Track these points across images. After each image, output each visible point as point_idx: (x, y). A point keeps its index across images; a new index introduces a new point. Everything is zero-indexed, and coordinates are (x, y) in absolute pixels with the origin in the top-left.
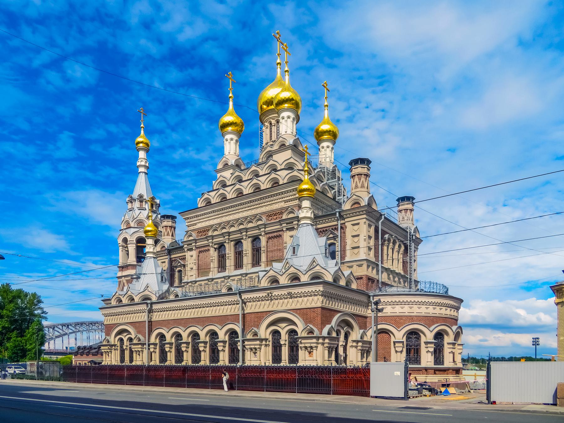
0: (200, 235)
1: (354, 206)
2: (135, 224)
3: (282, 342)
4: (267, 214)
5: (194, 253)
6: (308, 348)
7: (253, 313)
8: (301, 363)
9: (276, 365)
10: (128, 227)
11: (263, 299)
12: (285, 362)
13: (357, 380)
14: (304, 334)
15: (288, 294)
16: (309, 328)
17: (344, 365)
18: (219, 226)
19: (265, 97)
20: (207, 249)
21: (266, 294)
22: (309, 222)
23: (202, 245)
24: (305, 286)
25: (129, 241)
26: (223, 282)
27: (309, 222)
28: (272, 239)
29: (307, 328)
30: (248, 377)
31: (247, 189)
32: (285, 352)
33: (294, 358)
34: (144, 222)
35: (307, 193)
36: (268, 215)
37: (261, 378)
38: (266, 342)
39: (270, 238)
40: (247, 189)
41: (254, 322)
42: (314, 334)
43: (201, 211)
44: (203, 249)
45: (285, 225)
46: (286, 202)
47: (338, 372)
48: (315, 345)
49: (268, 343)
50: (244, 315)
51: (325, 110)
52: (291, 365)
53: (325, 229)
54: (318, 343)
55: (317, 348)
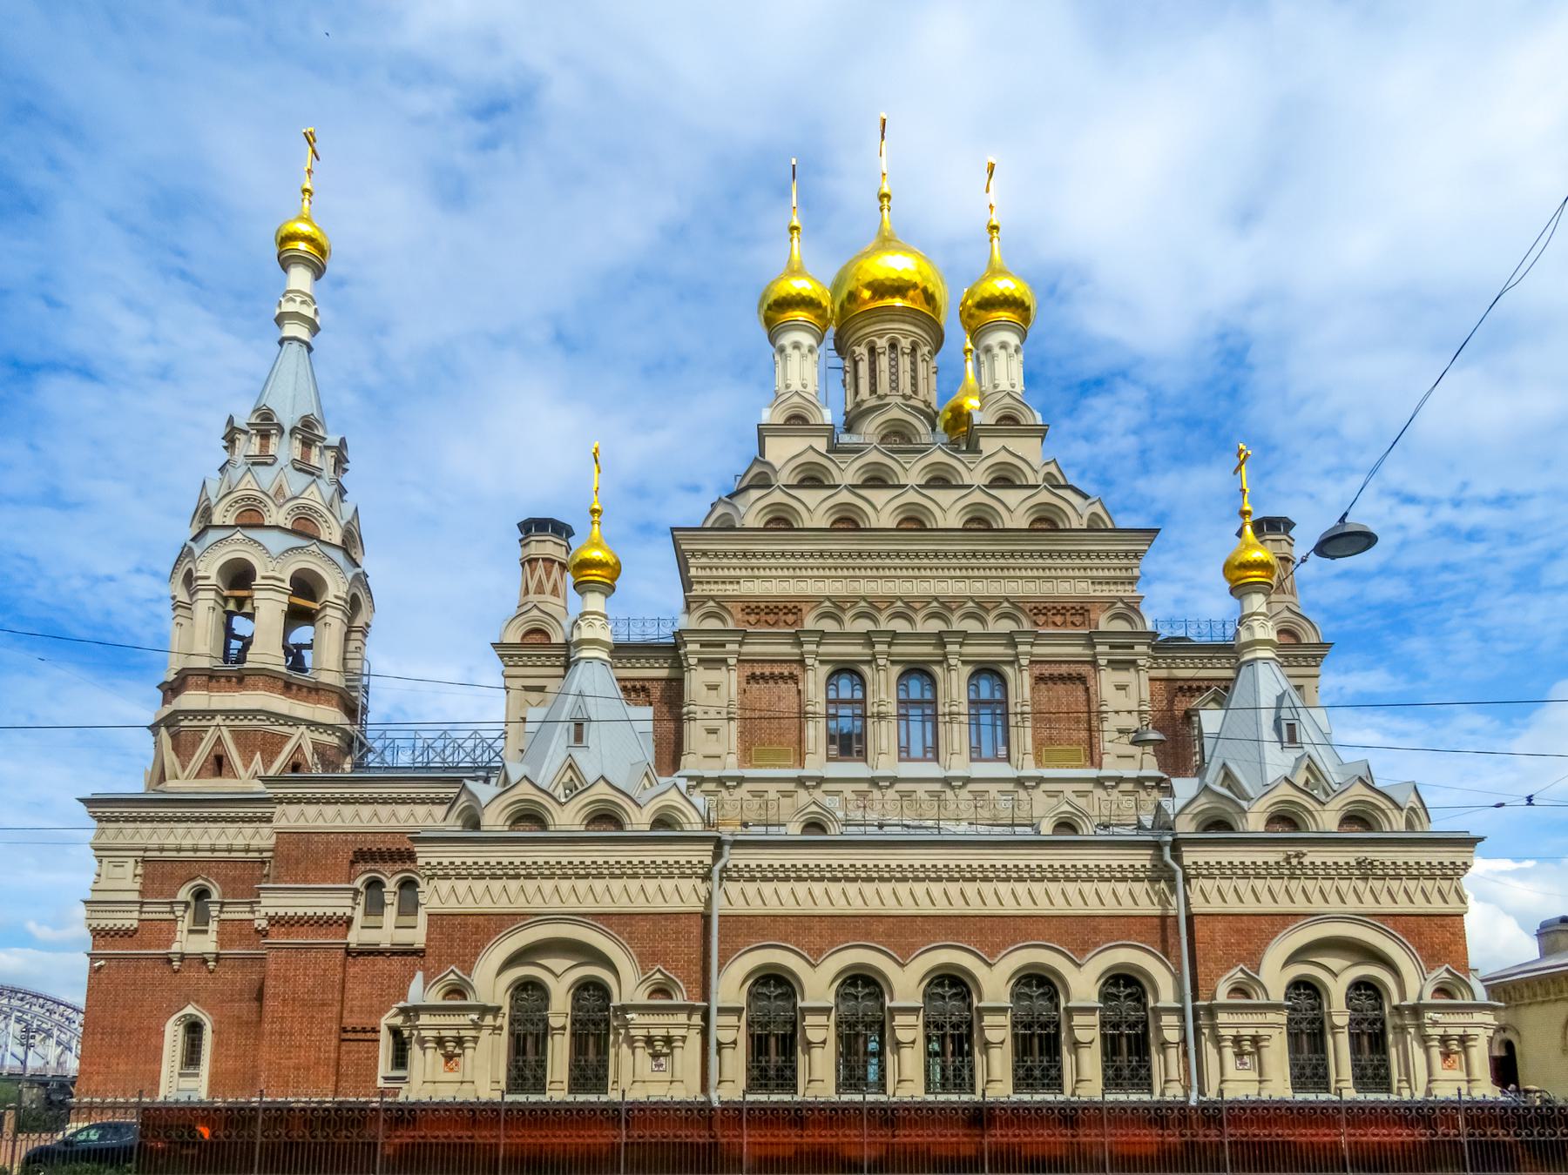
0: (752, 618)
1: (529, 640)
2: (227, 511)
3: (555, 1022)
4: (1033, 605)
5: (730, 680)
6: (447, 1044)
7: (1219, 915)
8: (1401, 1093)
9: (1026, 1098)
10: (246, 521)
11: (1298, 872)
12: (558, 1089)
13: (303, 1143)
14: (641, 997)
15: (1359, 863)
16: (456, 978)
17: (1406, 1095)
18: (886, 605)
19: (867, 271)
20: (786, 673)
21: (1280, 857)
22: (1270, 654)
23: (779, 655)
24: (1191, 846)
25: (264, 578)
26: (787, 794)
27: (1270, 654)
28: (1049, 682)
29: (448, 978)
30: (357, 1144)
31: (882, 509)
32: (559, 1053)
33: (589, 1073)
34: (320, 519)
35: (599, 572)
36: (1035, 608)
37: (316, 1144)
38: (495, 1018)
39: (1041, 679)
40: (948, 510)
41: (1227, 944)
42: (466, 999)
43: (943, 541)
44: (767, 670)
45: (1106, 649)
46: (1096, 581)
47: (547, 1121)
48: (683, 1032)
49: (499, 1022)
50: (1190, 918)
51: (966, 361)
52: (581, 1098)
53: (1195, 685)
54: (689, 1027)
55: (476, 1043)
